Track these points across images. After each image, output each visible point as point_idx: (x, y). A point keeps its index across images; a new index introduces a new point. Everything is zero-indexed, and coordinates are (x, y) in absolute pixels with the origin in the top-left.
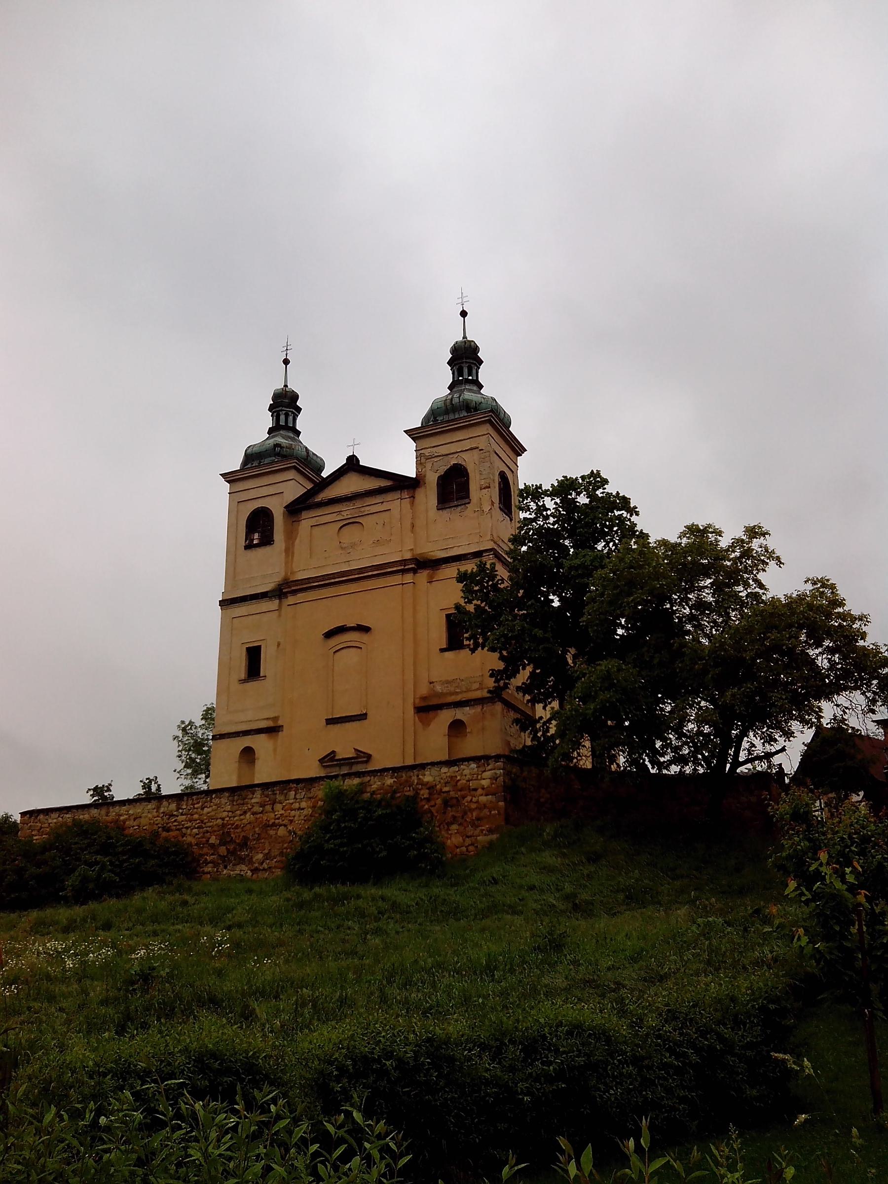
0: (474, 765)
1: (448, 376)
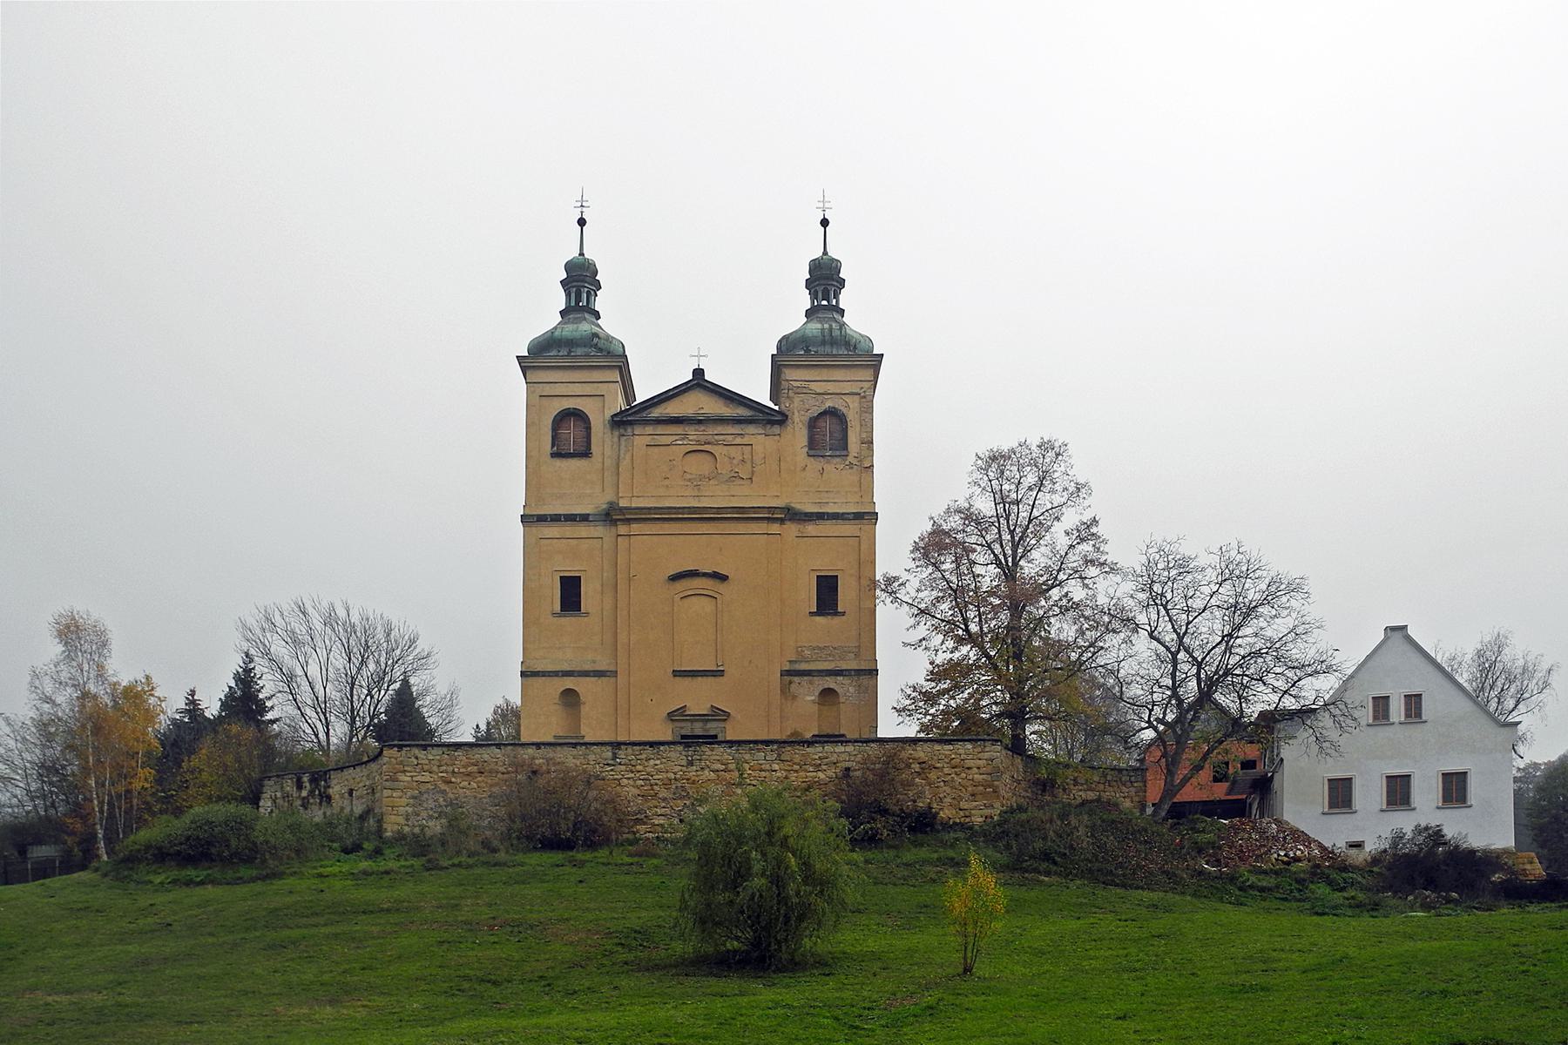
0: (969, 746)
1: (559, 300)
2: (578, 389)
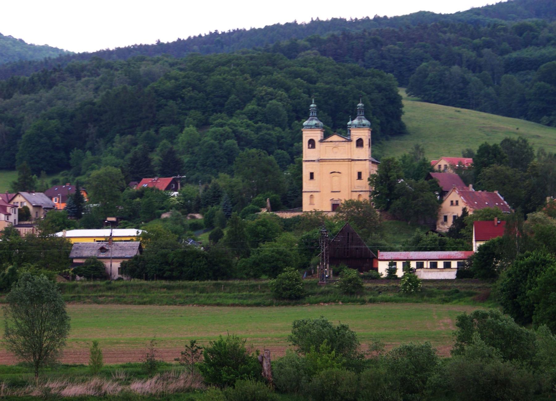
2: (312, 135)
